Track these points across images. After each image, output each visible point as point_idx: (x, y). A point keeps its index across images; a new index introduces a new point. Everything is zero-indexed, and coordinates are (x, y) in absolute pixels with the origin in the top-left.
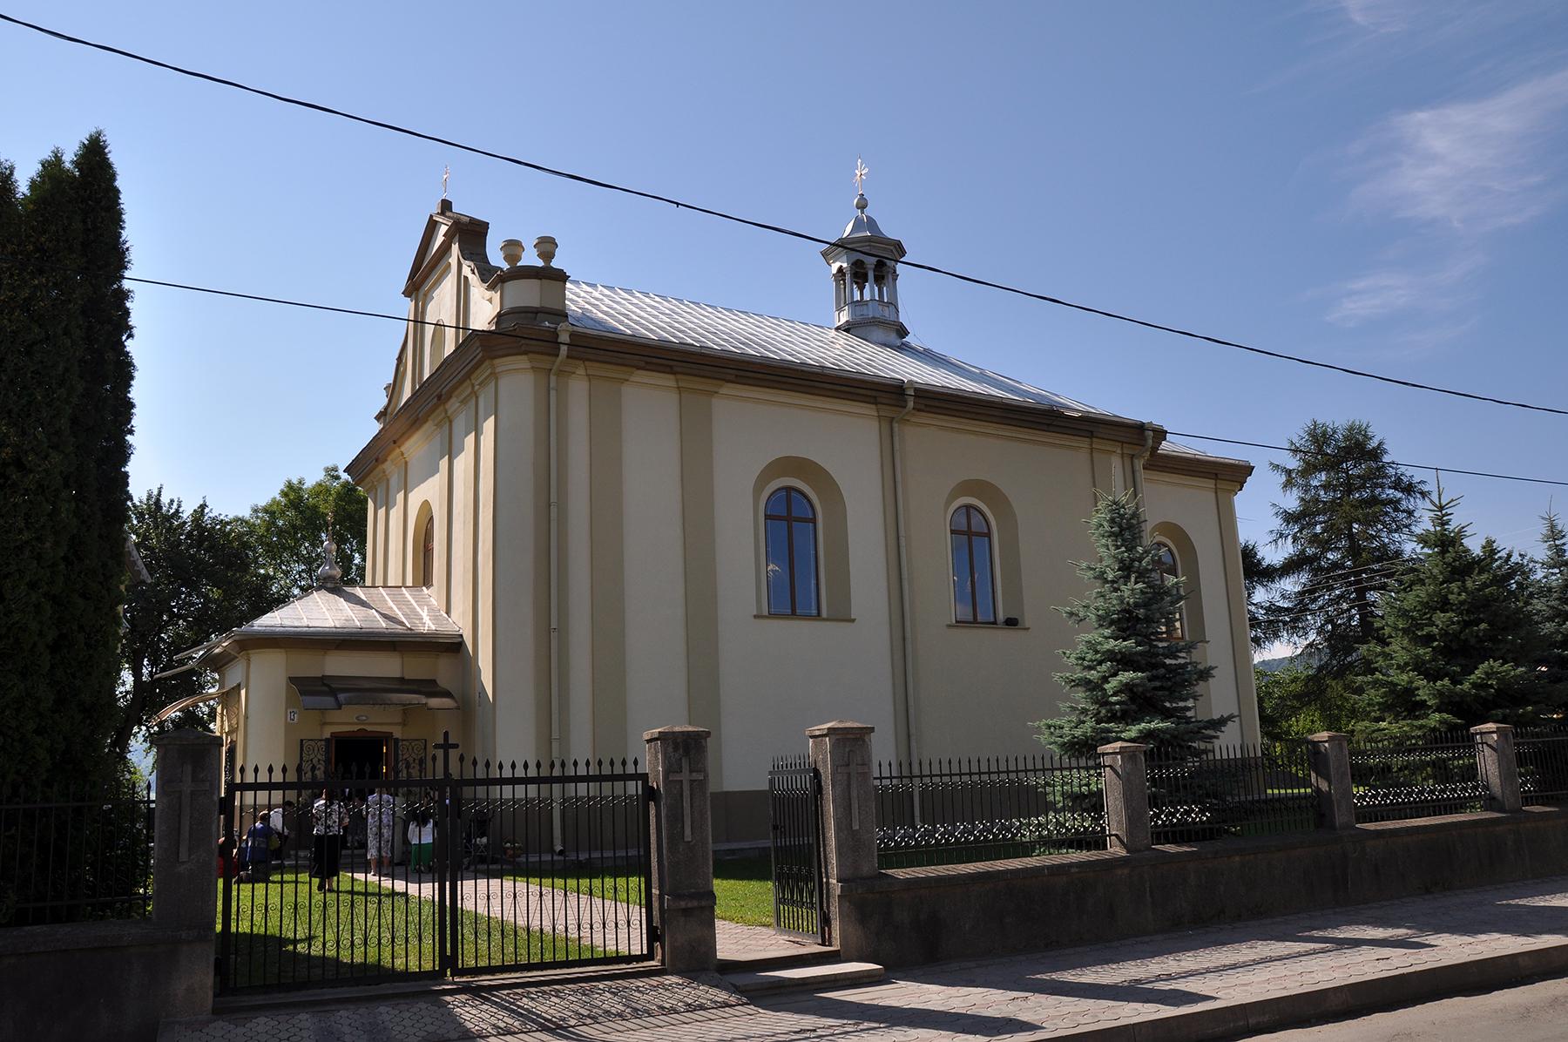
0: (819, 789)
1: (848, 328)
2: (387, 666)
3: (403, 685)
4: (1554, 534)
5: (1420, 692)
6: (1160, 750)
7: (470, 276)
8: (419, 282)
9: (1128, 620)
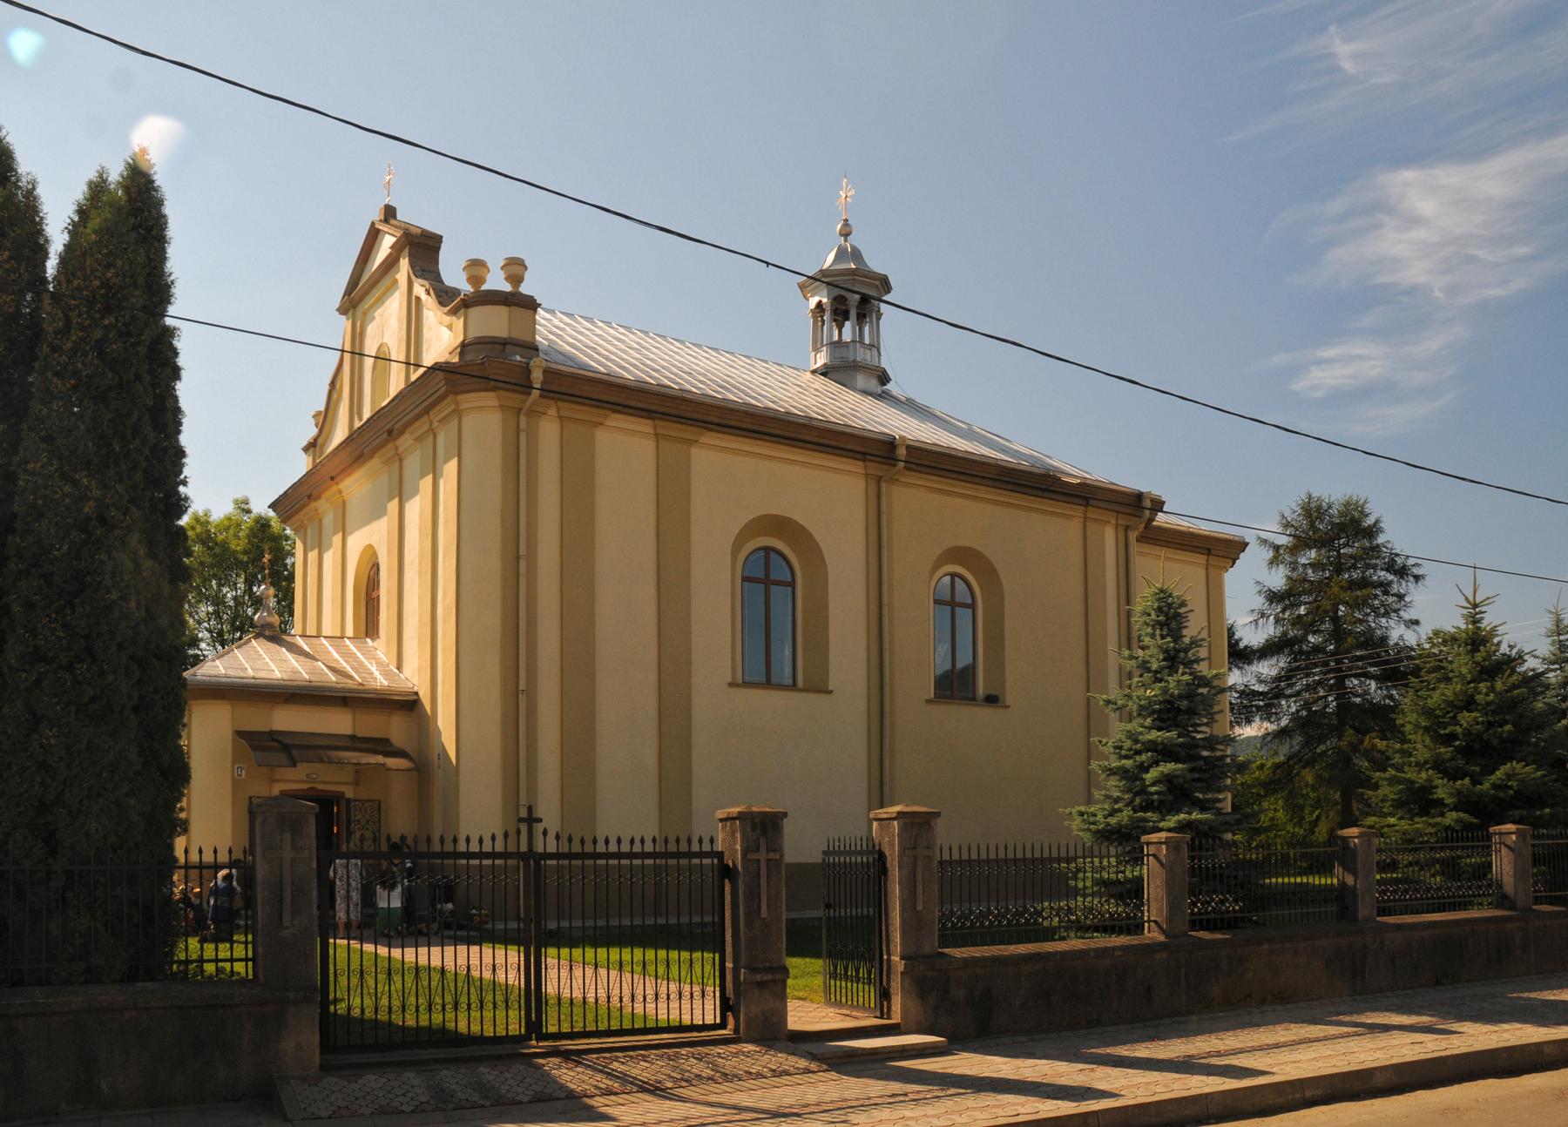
0: (883, 870)
1: (825, 372)
2: (338, 723)
3: (355, 742)
4: (1559, 628)
5: (1439, 790)
6: (1200, 838)
7: (424, 297)
8: (357, 298)
9: (1168, 711)
